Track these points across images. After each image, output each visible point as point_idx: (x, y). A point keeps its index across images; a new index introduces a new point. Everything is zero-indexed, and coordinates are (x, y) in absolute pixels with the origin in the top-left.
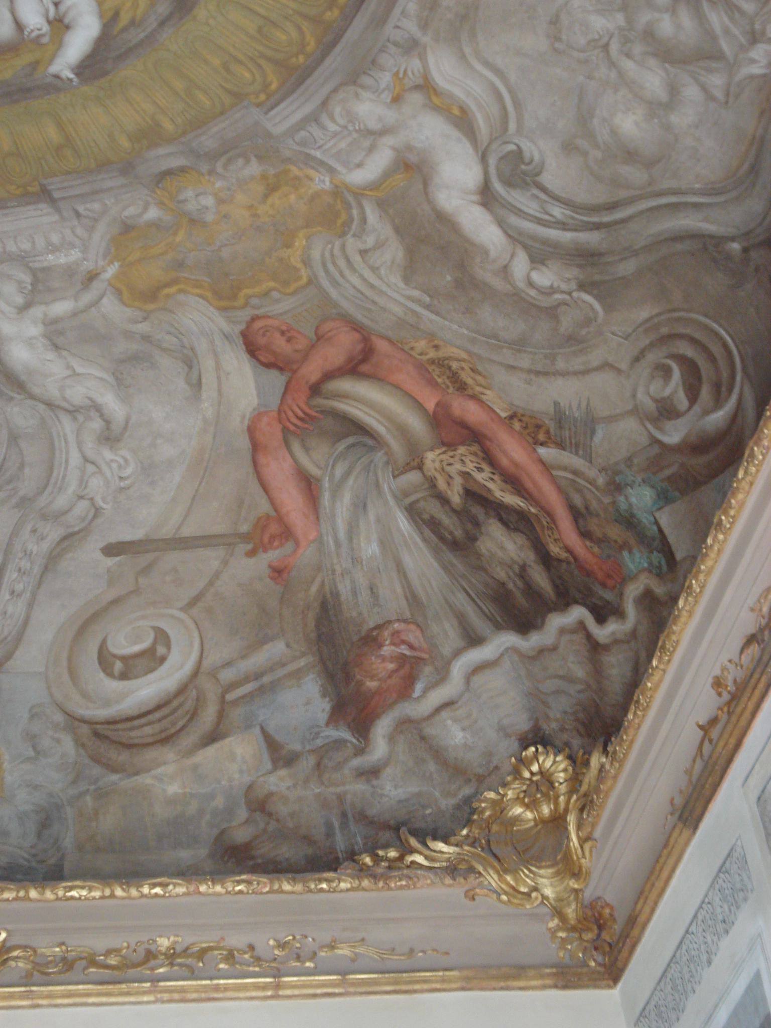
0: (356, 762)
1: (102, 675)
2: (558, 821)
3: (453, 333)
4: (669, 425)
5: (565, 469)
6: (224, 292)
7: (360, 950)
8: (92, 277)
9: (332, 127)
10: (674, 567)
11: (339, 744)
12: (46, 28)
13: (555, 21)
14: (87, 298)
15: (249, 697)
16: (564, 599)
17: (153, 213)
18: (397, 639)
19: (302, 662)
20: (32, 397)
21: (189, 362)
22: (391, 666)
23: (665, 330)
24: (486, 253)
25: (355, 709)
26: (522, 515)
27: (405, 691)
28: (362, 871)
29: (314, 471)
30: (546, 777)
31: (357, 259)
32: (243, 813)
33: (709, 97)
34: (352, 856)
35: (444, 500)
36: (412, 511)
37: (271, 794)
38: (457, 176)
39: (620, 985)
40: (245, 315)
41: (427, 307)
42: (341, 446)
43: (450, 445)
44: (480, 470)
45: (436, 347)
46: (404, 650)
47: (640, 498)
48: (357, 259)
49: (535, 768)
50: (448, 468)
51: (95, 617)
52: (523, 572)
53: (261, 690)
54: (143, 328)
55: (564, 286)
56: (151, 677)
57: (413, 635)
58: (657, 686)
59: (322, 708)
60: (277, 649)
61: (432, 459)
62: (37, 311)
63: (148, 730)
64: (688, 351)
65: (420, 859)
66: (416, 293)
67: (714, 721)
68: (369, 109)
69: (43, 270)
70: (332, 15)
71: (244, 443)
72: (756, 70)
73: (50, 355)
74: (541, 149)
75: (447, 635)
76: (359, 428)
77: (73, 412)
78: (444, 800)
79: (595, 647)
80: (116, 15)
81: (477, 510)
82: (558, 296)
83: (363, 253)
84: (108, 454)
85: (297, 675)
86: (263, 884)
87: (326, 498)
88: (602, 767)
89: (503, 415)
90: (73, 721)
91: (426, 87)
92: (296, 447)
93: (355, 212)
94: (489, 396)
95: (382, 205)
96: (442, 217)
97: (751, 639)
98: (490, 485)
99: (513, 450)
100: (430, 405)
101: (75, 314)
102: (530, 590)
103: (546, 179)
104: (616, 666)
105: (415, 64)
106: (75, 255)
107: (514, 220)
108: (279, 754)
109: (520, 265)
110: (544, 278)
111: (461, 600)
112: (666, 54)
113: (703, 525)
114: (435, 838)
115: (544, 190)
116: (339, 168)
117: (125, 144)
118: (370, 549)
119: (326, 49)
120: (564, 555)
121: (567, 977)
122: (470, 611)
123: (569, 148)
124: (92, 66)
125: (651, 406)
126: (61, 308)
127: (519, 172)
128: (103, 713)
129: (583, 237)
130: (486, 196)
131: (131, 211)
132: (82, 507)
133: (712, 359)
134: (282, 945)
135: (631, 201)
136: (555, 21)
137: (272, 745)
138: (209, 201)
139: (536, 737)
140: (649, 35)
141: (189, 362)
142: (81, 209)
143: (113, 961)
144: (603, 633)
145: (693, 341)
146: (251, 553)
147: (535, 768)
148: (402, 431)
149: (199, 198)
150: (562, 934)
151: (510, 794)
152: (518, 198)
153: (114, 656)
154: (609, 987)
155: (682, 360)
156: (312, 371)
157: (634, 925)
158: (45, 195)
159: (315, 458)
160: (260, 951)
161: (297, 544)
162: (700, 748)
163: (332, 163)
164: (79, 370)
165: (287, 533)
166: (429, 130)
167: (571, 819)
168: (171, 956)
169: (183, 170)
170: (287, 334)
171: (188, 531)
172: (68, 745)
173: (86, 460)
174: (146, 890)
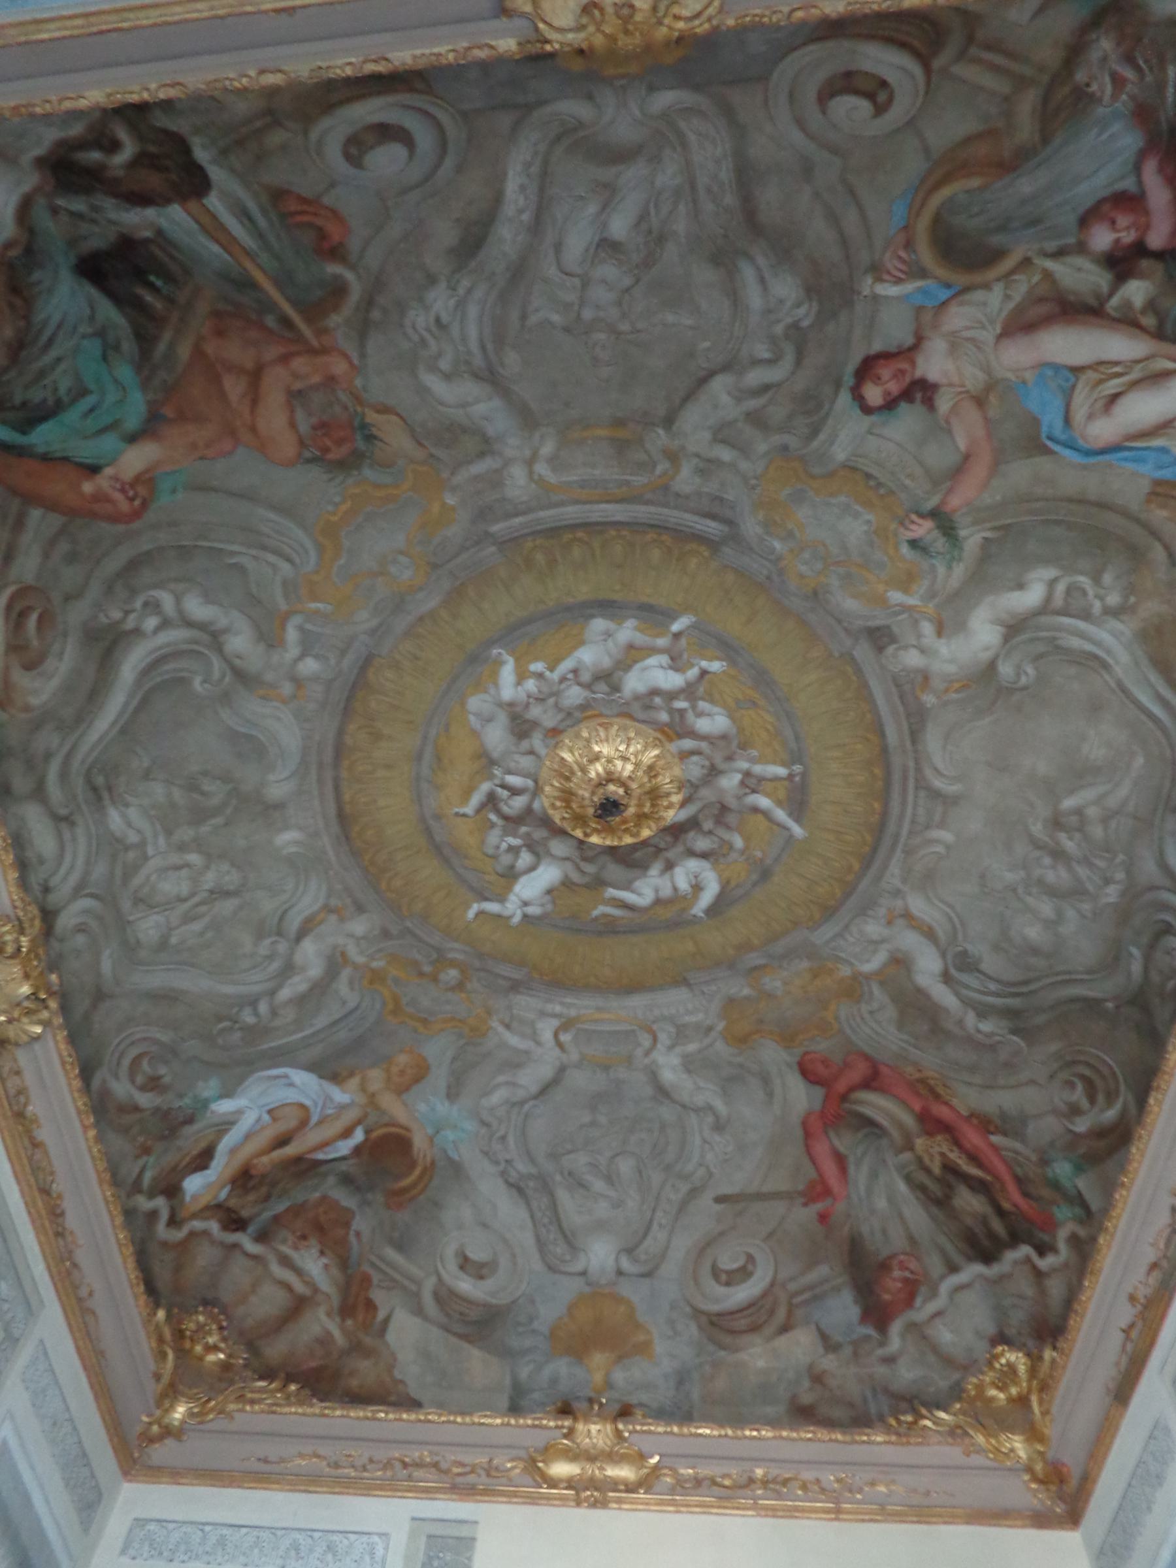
0: (880, 1352)
1: (713, 1283)
2: (1022, 1401)
3: (929, 1061)
4: (1078, 1120)
5: (1010, 1150)
6: (787, 1038)
7: (893, 1488)
8: (710, 1029)
9: (851, 939)
10: (1092, 1218)
11: (867, 1338)
12: (690, 890)
13: (982, 877)
14: (707, 1041)
15: (806, 1303)
16: (1015, 1239)
17: (746, 991)
18: (903, 1267)
19: (840, 1280)
20: (674, 1101)
21: (766, 1080)
22: (899, 1285)
23: (1068, 1058)
24: (947, 1011)
25: (878, 1315)
26: (982, 1182)
27: (909, 1302)
28: (889, 1430)
29: (842, 1150)
30: (1012, 1368)
31: (867, 1016)
32: (806, 1384)
33: (1083, 917)
34: (882, 1418)
35: (928, 1171)
36: (908, 1179)
37: (824, 1372)
38: (928, 966)
39: (1082, 1528)
40: (799, 1051)
41: (915, 1047)
42: (860, 1135)
43: (930, 1134)
44: (952, 1151)
45: (920, 1071)
46: (907, 1274)
47: (1062, 1169)
48: (867, 1016)
49: (1003, 1361)
50: (931, 1150)
51: (708, 1244)
52: (985, 1222)
53: (816, 1298)
54: (739, 1059)
55: (1000, 1032)
56: (744, 1286)
57: (913, 1265)
58: (1089, 1299)
59: (855, 1312)
60: (823, 1270)
61: (920, 1143)
62: (678, 1050)
63: (743, 1322)
64: (1087, 1072)
65: (928, 1423)
66: (905, 1037)
67: (1132, 1326)
68: (873, 929)
69: (684, 1025)
70: (850, 878)
71: (799, 1133)
72: (1111, 900)
73: (685, 1076)
74: (978, 949)
75: (935, 1265)
76: (870, 1123)
77: (697, 1110)
78: (942, 1382)
79: (1039, 1274)
80: (728, 882)
81: (951, 1179)
82: (998, 1038)
83: (871, 1012)
84: (717, 1138)
85: (837, 1289)
86: (823, 1434)
87: (852, 1169)
88: (1053, 1361)
89: (965, 1113)
90: (697, 1313)
91: (907, 915)
92: (832, 1134)
93: (866, 988)
94: (955, 1102)
95: (882, 984)
96: (919, 991)
97: (1154, 1266)
98: (960, 1162)
99: (973, 1138)
100: (917, 1107)
101: (700, 1051)
102: (992, 1235)
103: (984, 967)
104: (1056, 1288)
105: (899, 903)
106: (701, 1016)
107: (964, 992)
108: (829, 1344)
109: (971, 1019)
110: (986, 1027)
111: (943, 1240)
112: (1053, 892)
113: (1109, 1187)
114: (939, 1408)
115: (984, 974)
116: (856, 963)
117: (731, 952)
118: (881, 1203)
119: (847, 895)
120: (1013, 1209)
121: (1041, 1520)
122: (949, 1247)
123: (996, 948)
124: (714, 910)
125: (1062, 1107)
126: (692, 1047)
127: (966, 963)
128: (715, 1308)
129: (1010, 1001)
130: (946, 978)
131: (733, 991)
132: (701, 1172)
133: (1103, 1077)
134: (839, 1481)
135: (1038, 979)
136: (982, 877)
137: (824, 1337)
138: (778, 984)
139: (1001, 1338)
140: (1040, 882)
141: (766, 1080)
142: (705, 990)
143: (727, 1482)
144: (1044, 1264)
145: (1087, 1064)
146: (805, 1205)
147: (1003, 1361)
148: (900, 1126)
149: (773, 982)
150: (1033, 1486)
151: (987, 1379)
152: (965, 978)
153: (722, 1271)
154: (1072, 1529)
155: (1083, 1077)
156: (841, 1086)
157: (1087, 1481)
158: (685, 982)
159: (843, 1142)
160: (824, 1484)
161: (835, 1199)
162: (1124, 1346)
163: (853, 960)
164: (702, 1084)
165: (827, 1192)
166: (910, 940)
167: (1034, 1399)
168: (765, 1483)
169: (765, 966)
170: (825, 1062)
171: (765, 1189)
172: (694, 1329)
173: (705, 1141)
174: (747, 1433)
